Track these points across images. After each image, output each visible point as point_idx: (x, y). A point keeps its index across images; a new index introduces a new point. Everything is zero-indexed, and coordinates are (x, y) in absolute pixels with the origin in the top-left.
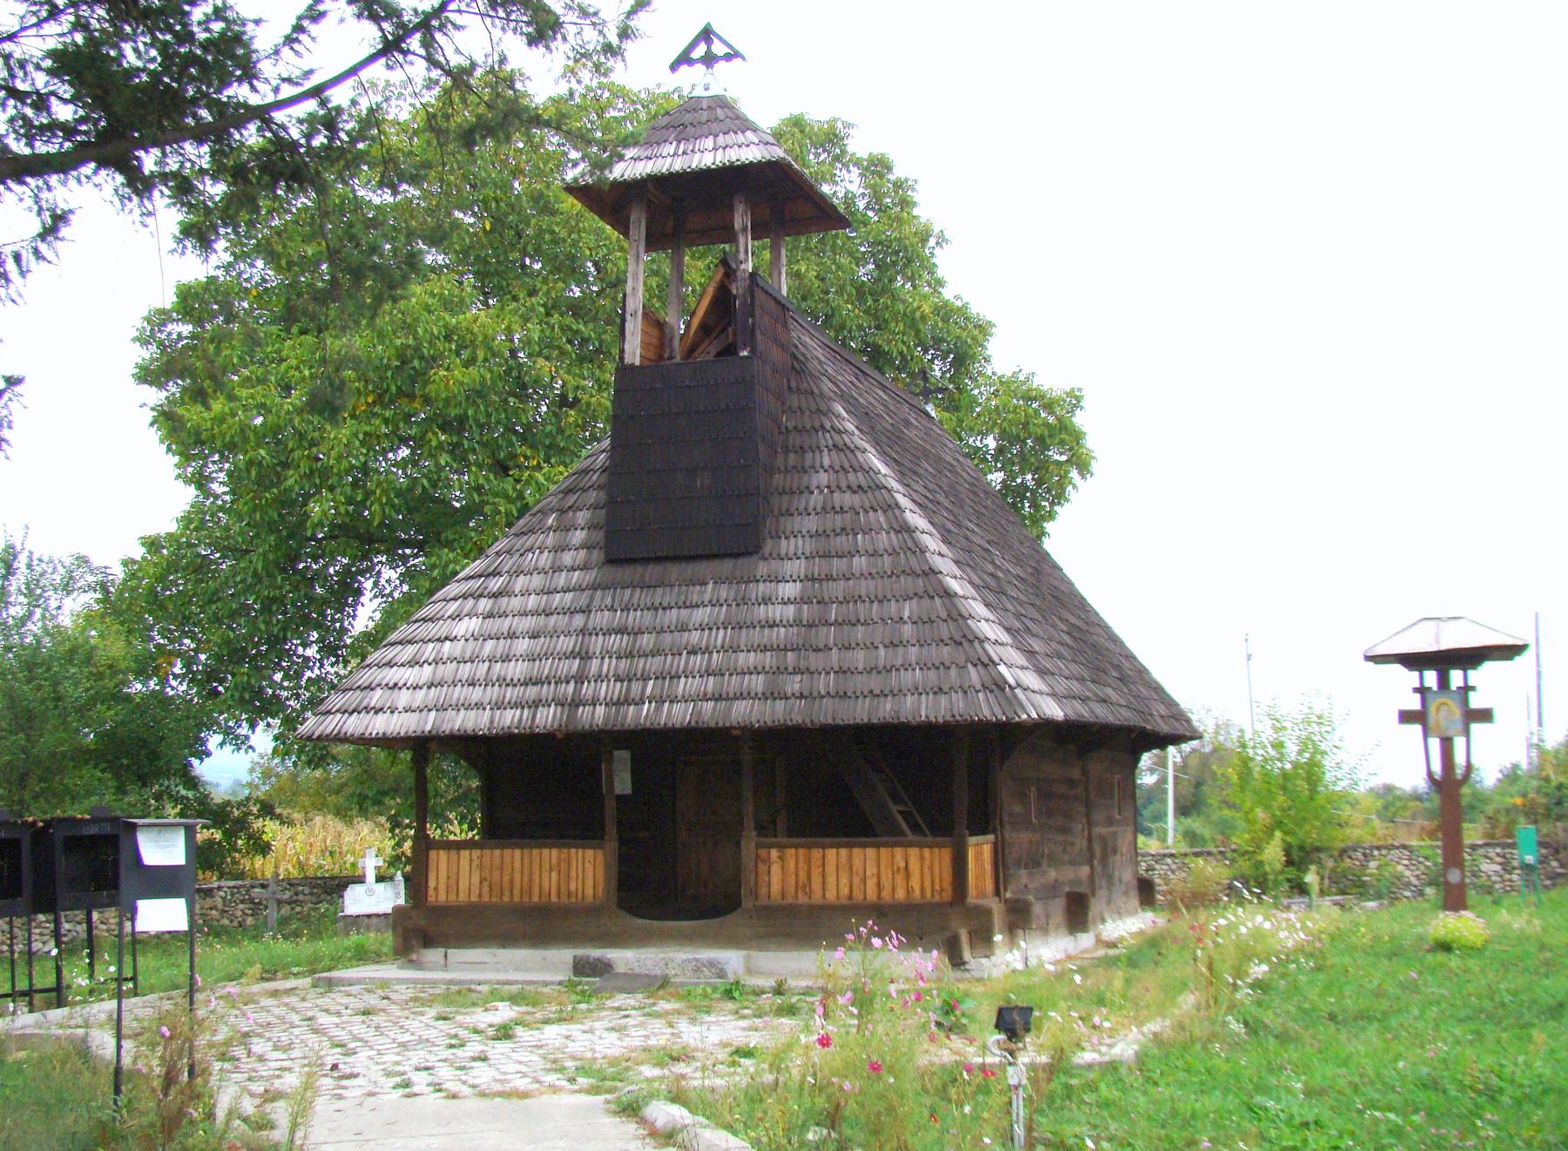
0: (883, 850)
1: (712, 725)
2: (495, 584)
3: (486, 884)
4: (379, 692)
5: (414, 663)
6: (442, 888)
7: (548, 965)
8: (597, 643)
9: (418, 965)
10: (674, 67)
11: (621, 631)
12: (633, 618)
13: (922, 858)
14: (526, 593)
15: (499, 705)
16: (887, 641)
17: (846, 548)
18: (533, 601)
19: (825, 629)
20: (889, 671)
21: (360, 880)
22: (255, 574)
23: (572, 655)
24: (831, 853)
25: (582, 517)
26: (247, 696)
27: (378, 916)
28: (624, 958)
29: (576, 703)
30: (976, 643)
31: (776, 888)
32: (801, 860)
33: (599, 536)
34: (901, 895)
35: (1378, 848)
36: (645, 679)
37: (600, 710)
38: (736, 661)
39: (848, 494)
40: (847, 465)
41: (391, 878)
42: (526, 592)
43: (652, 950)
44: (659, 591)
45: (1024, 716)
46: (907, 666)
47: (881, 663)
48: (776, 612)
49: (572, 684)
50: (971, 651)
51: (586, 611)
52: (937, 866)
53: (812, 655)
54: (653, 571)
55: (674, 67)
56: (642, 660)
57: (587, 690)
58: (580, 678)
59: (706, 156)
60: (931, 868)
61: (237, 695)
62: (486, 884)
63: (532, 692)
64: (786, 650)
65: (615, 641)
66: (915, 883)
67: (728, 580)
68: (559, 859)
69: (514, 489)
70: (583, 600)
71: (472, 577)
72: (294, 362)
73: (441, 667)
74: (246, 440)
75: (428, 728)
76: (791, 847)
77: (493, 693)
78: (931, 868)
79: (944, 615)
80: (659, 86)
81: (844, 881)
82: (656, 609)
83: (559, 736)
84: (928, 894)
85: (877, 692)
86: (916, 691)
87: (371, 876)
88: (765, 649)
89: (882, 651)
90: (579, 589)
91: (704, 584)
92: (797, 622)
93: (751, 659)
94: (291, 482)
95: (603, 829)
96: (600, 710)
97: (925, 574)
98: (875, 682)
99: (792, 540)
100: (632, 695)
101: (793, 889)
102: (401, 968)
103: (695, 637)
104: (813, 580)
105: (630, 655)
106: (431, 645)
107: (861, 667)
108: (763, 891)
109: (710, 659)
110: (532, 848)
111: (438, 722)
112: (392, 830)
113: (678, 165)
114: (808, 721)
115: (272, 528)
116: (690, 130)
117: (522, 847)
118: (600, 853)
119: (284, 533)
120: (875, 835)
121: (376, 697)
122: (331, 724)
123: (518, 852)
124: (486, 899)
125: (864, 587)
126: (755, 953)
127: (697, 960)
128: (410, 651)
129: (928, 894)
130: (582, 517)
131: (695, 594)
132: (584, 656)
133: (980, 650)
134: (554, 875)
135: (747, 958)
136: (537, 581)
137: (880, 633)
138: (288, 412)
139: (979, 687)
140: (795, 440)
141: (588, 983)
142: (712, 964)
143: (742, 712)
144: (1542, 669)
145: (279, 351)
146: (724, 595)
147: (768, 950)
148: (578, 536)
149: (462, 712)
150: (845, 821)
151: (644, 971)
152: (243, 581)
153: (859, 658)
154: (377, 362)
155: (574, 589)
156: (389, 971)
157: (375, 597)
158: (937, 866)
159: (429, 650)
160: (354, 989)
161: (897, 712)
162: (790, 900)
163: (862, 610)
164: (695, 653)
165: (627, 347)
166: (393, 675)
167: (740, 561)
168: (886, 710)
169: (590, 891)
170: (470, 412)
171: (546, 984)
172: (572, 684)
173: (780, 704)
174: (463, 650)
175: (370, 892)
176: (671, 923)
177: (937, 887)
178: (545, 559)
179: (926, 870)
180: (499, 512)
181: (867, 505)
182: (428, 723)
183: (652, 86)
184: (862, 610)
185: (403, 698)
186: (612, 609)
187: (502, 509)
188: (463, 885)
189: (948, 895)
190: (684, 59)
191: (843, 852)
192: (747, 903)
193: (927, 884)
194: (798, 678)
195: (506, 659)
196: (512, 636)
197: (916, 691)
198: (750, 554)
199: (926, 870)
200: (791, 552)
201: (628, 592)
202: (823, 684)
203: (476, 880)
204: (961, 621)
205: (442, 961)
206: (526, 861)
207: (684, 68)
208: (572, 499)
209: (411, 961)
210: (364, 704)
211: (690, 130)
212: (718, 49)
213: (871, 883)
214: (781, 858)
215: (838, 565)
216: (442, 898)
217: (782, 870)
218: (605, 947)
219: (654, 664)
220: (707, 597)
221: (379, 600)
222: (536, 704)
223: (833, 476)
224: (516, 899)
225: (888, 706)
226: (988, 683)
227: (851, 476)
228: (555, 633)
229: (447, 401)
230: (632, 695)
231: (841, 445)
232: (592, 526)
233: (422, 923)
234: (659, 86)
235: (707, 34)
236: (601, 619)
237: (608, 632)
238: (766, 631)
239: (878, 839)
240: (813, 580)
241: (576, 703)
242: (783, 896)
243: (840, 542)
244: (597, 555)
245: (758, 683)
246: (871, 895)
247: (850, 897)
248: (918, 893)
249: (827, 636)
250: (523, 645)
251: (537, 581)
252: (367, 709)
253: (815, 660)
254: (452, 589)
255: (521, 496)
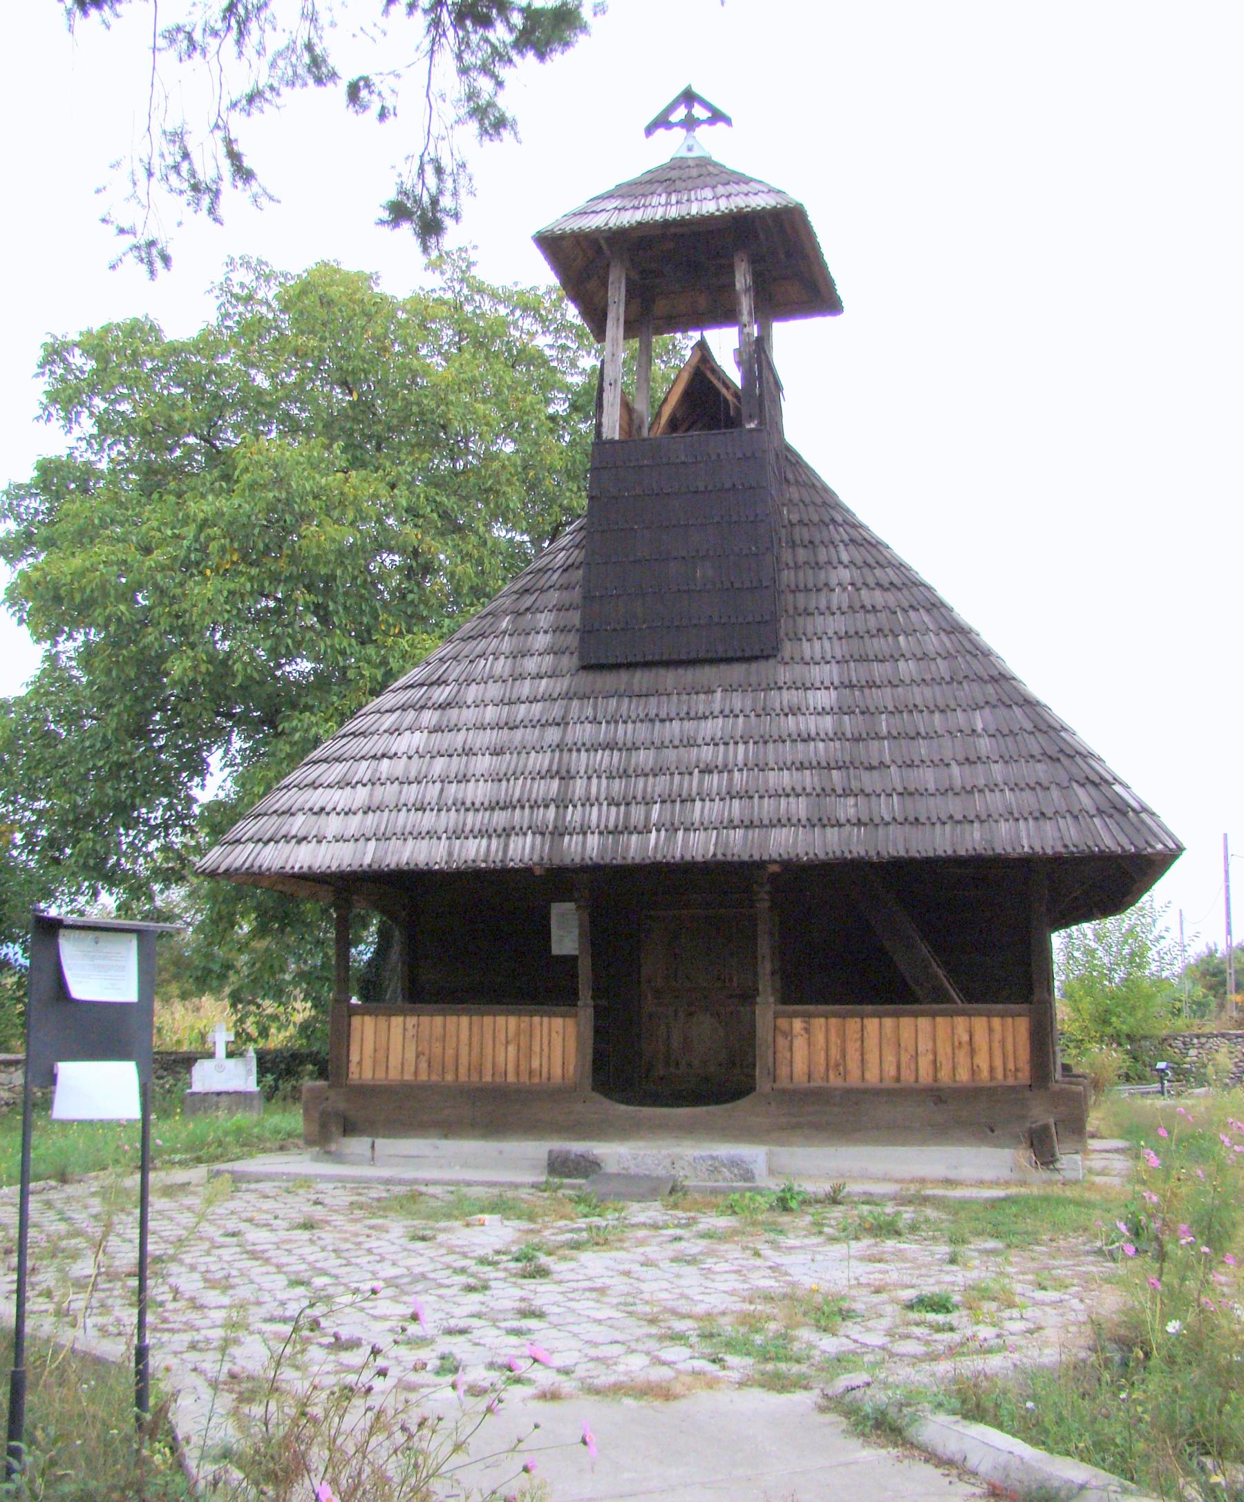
0: (939, 1020)
1: (746, 858)
2: (441, 694)
3: (423, 1059)
4: (300, 818)
5: (344, 783)
6: (368, 1064)
7: (518, 1159)
8: (581, 761)
9: (338, 1158)
10: (649, 131)
11: (610, 746)
12: (623, 732)
13: (991, 1030)
14: (480, 704)
15: (458, 834)
16: (960, 758)
17: (887, 652)
18: (490, 713)
19: (876, 743)
20: (971, 792)
21: (211, 1055)
22: (104, 738)
23: (549, 774)
24: (872, 1024)
25: (544, 620)
26: (92, 862)
27: (228, 1093)
28: (615, 1153)
29: (559, 832)
30: (1078, 759)
31: (800, 1067)
32: (833, 1031)
33: (572, 640)
34: (963, 1075)
35: (1198, 1037)
36: (648, 803)
37: (593, 841)
38: (766, 781)
39: (878, 593)
40: (871, 561)
41: (241, 1055)
42: (481, 704)
43: (641, 1144)
44: (653, 701)
45: (1159, 847)
46: (993, 787)
47: (958, 784)
48: (810, 724)
49: (552, 808)
50: (1074, 770)
51: (562, 723)
52: (1010, 1039)
53: (865, 776)
54: (641, 679)
55: (649, 131)
56: (641, 781)
57: (573, 816)
58: (562, 803)
59: (705, 204)
60: (1003, 1042)
61: (81, 861)
62: (423, 1059)
63: (500, 818)
64: (829, 767)
65: (602, 758)
66: (982, 1061)
67: (742, 687)
68: (518, 1033)
69: (378, 654)
70: (556, 710)
71: (411, 686)
72: (155, 524)
73: (379, 790)
74: (106, 595)
75: (367, 861)
76: (819, 1016)
77: (450, 819)
78: (1003, 1042)
79: (1029, 726)
80: (516, 284)
81: (890, 1059)
82: (652, 721)
83: (538, 872)
84: (999, 1074)
85: (959, 817)
86: (1012, 816)
87: (221, 1051)
88: (802, 767)
89: (955, 769)
90: (549, 698)
91: (710, 691)
92: (839, 736)
93: (787, 779)
94: (151, 638)
95: (576, 994)
96: (593, 841)
97: (993, 679)
98: (954, 806)
99: (817, 644)
100: (633, 822)
101: (822, 1069)
102: (316, 1159)
103: (707, 753)
104: (851, 686)
105: (625, 774)
106: (364, 764)
107: (931, 787)
108: (783, 1071)
109: (731, 780)
110: (482, 1015)
111: (380, 853)
112: (234, 1005)
113: (673, 213)
114: (872, 853)
115: (126, 686)
116: (679, 184)
117: (470, 1013)
118: (570, 1022)
119: (140, 693)
120: (916, 1001)
121: (298, 824)
122: (239, 857)
123: (465, 1020)
124: (423, 1077)
125: (918, 695)
126: (777, 1149)
127: (712, 1158)
128: (337, 771)
129: (999, 1074)
130: (544, 620)
131: (700, 703)
132: (566, 776)
133: (1085, 767)
134: (512, 1049)
135: (770, 1155)
136: (494, 691)
137: (948, 748)
138: (150, 568)
139: (1093, 811)
140: (802, 534)
141: (572, 1187)
142: (734, 1163)
143: (783, 843)
144: (1231, 884)
145: (139, 515)
146: (738, 706)
147: (791, 1144)
148: (541, 641)
149: (410, 842)
150: (869, 981)
151: (642, 1171)
152: (92, 746)
153: (928, 778)
154: (245, 520)
155: (543, 699)
156: (301, 1163)
157: (226, 766)
158: (1010, 1039)
159: (363, 770)
160: (266, 1186)
161: (991, 842)
162: (817, 1083)
163: (921, 722)
164: (711, 772)
165: (605, 420)
166: (317, 798)
167: (754, 666)
168: (973, 840)
169: (557, 1071)
170: (339, 572)
171: (516, 1186)
172: (552, 808)
173: (832, 833)
174: (407, 768)
175: (220, 1068)
176: (665, 1110)
177: (1011, 1066)
178: (501, 666)
179: (996, 1045)
180: (363, 676)
181: (906, 604)
182: (367, 856)
183: (509, 285)
184: (921, 722)
185: (333, 825)
186: (595, 721)
187: (366, 673)
188: (394, 1061)
189: (1024, 1077)
190: (662, 122)
191: (888, 1022)
192: (763, 1084)
193: (998, 1063)
194: (851, 801)
195: (463, 779)
196: (468, 752)
197: (1012, 816)
198: (767, 658)
199: (996, 1045)
200: (818, 657)
201: (613, 702)
202: (886, 808)
203: (411, 1055)
204: (1052, 733)
205: (368, 1153)
206: (475, 1029)
207: (661, 132)
208: (528, 600)
209: (328, 1153)
210: (283, 832)
211: (679, 184)
212: (699, 112)
213: (925, 1063)
214: (807, 1030)
215: (879, 671)
216: (368, 1075)
217: (810, 1044)
218: (570, 1139)
219: (660, 785)
220: (717, 707)
221: (228, 770)
222: (507, 832)
223: (856, 573)
224: (463, 1078)
225: (977, 835)
226: (1105, 806)
227: (878, 572)
228: (523, 750)
229: (317, 559)
230: (633, 822)
231: (859, 539)
232: (558, 630)
233: (342, 1105)
234: (516, 284)
235: (689, 97)
236: (582, 732)
237: (593, 748)
238: (800, 746)
239: (915, 1007)
240: (851, 686)
241: (559, 832)
242: (992, 1078)
243: (878, 645)
244: (568, 662)
245: (800, 807)
246: (925, 1076)
247: (898, 1079)
248: (985, 1074)
249: (881, 751)
250: (483, 763)
251: (494, 691)
252: (286, 838)
253: (869, 781)
254: (387, 700)
255: (384, 662)
